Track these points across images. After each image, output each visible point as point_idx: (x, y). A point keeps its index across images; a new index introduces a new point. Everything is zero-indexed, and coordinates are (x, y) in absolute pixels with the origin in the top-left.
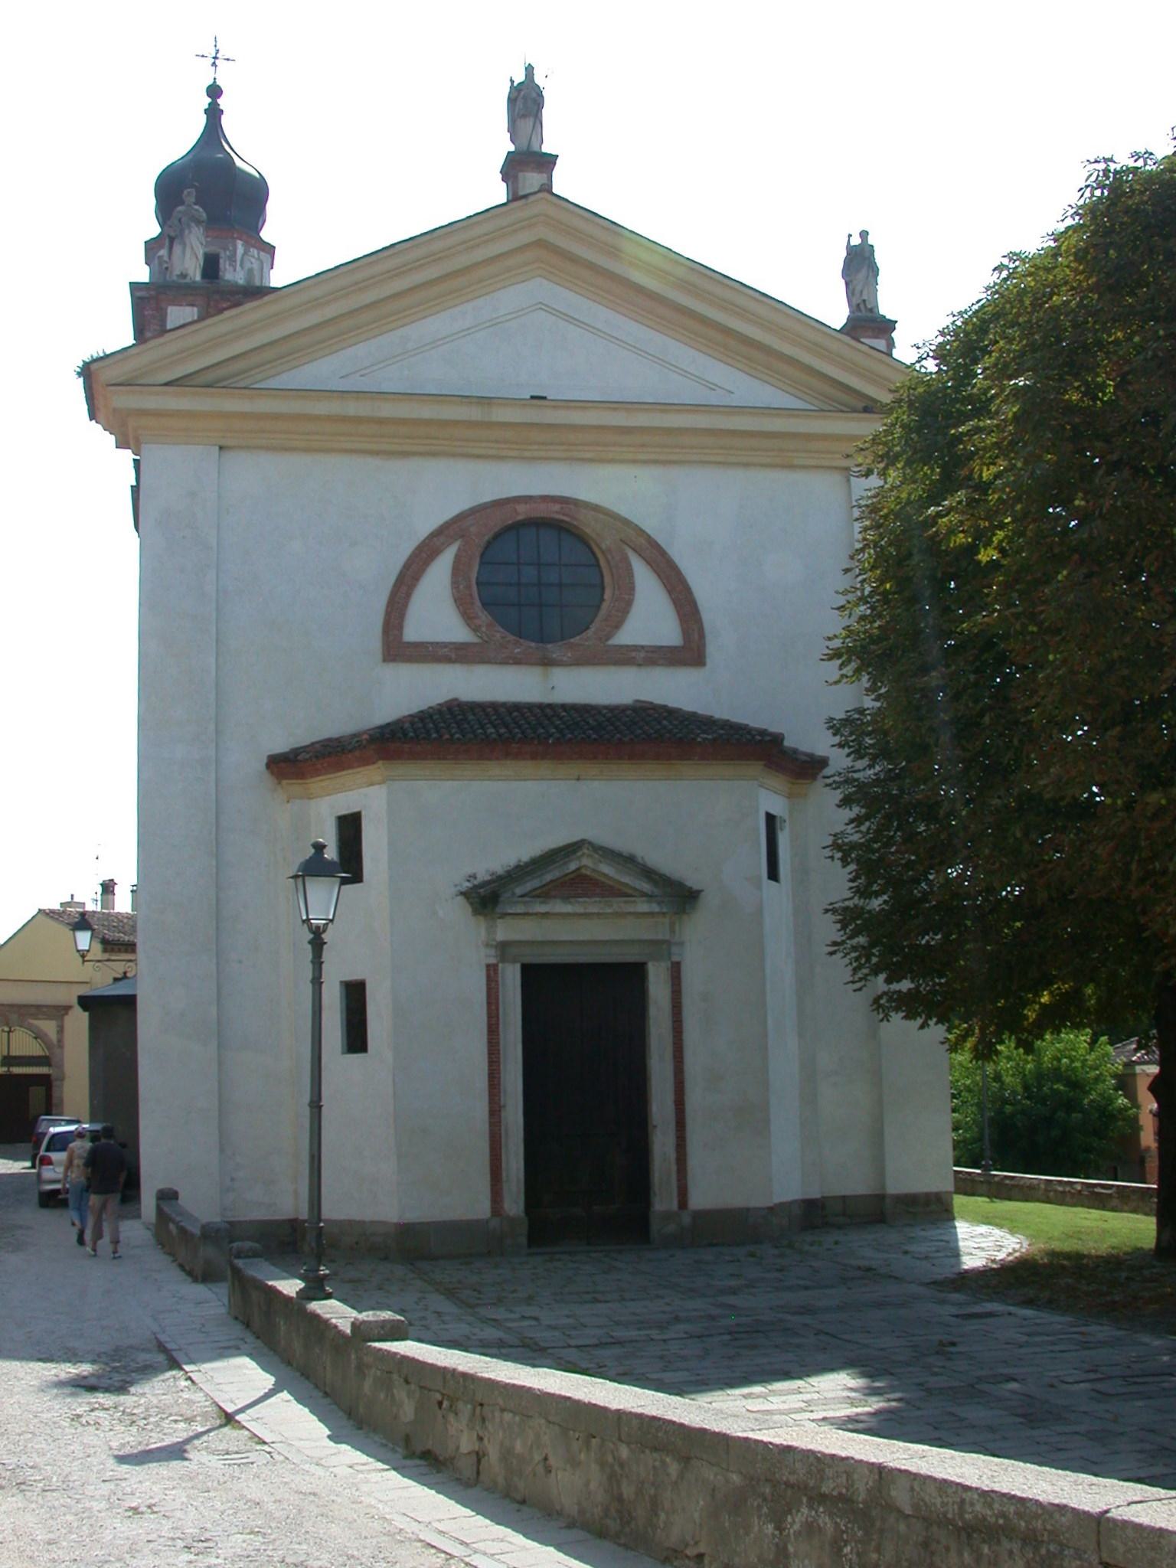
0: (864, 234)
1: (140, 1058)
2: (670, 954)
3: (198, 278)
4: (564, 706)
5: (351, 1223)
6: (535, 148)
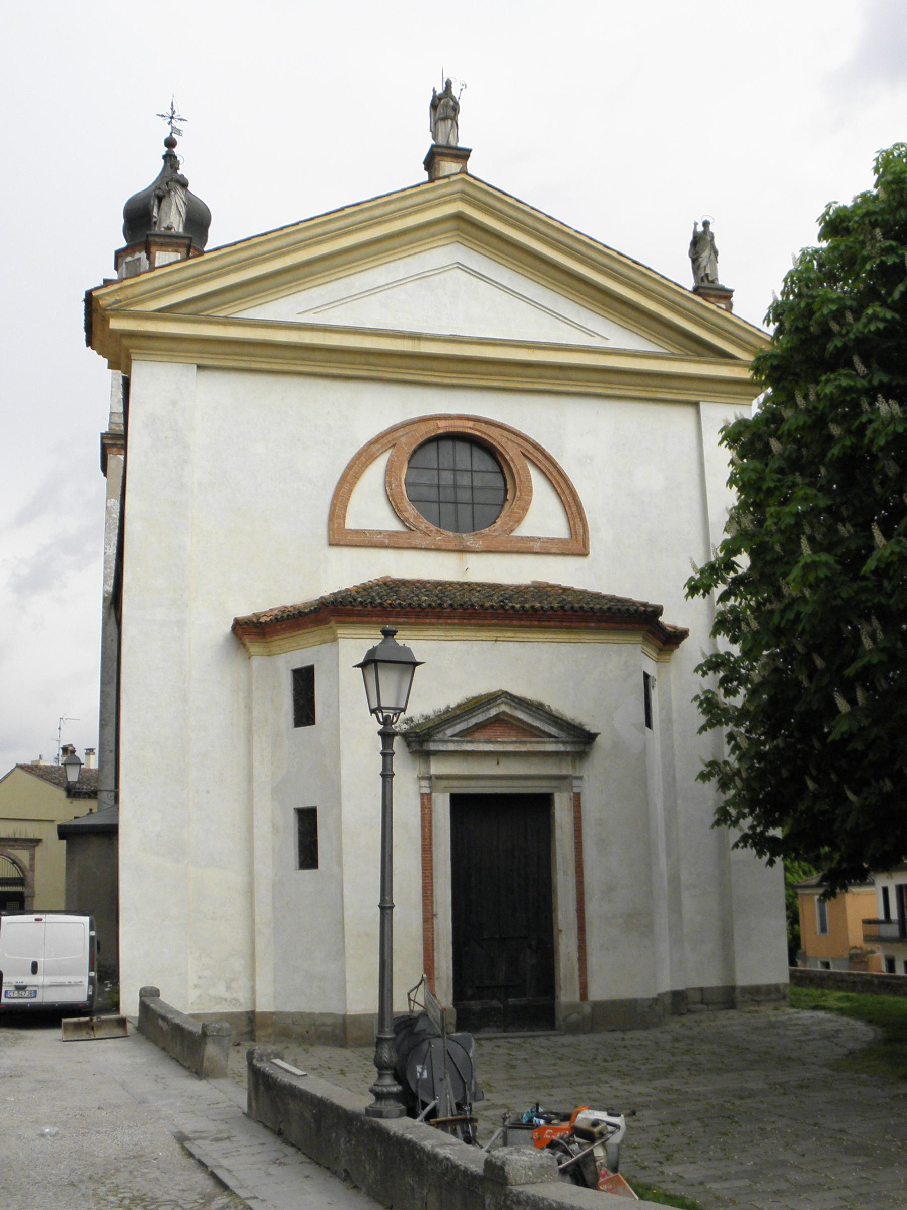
0: (706, 224)
1: (344, 745)
2: (572, 787)
3: (181, 230)
4: (477, 584)
5: (302, 1015)
6: (453, 143)
